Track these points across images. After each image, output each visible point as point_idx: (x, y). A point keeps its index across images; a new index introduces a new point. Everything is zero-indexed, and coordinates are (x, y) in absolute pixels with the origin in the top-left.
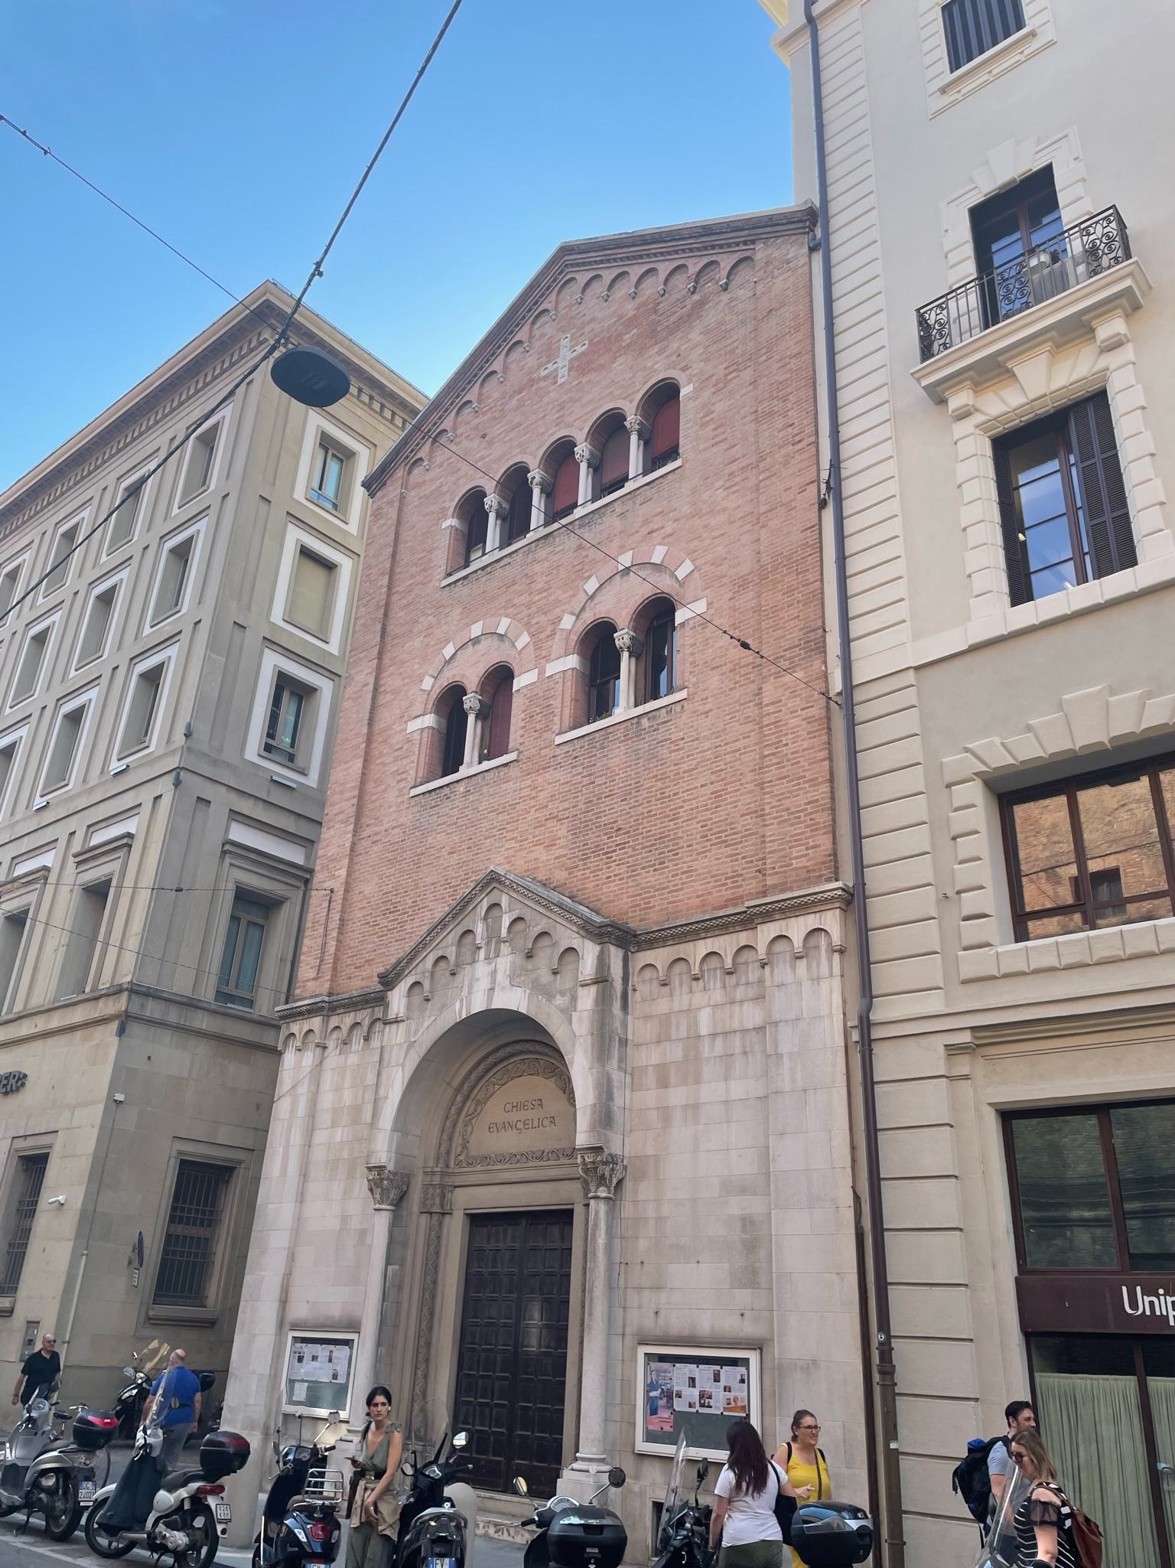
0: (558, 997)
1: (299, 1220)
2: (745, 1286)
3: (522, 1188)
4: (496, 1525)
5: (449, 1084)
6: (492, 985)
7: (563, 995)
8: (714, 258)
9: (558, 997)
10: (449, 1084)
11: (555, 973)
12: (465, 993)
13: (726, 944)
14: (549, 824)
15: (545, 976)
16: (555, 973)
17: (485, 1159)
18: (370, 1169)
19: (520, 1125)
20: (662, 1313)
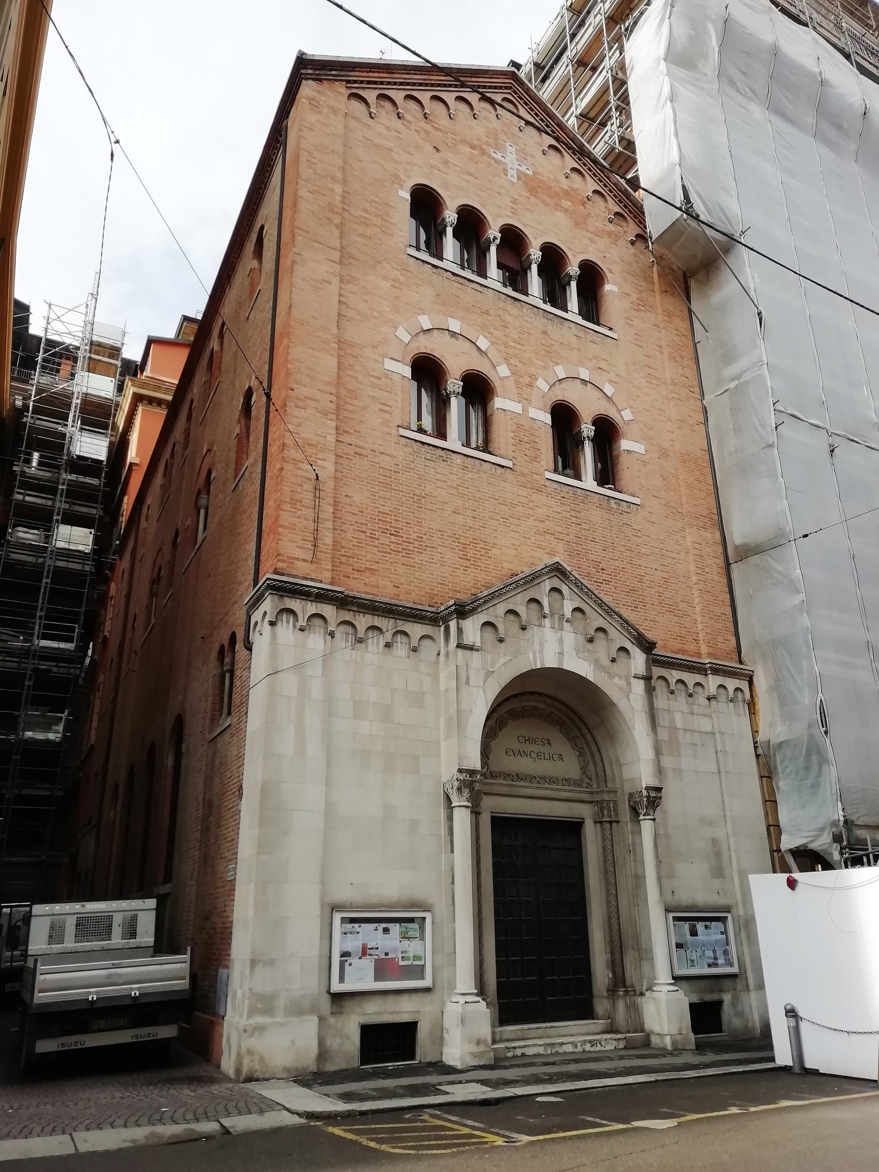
0: (617, 678)
1: (329, 806)
2: (716, 877)
3: (541, 803)
4: (590, 1042)
5: (722, 734)
6: (556, 647)
7: (620, 678)
8: (628, 218)
9: (617, 678)
10: (722, 734)
11: (613, 660)
12: (536, 647)
13: (691, 679)
14: (548, 536)
15: (606, 661)
16: (613, 660)
17: (507, 775)
18: (460, 771)
19: (533, 755)
20: (675, 893)
